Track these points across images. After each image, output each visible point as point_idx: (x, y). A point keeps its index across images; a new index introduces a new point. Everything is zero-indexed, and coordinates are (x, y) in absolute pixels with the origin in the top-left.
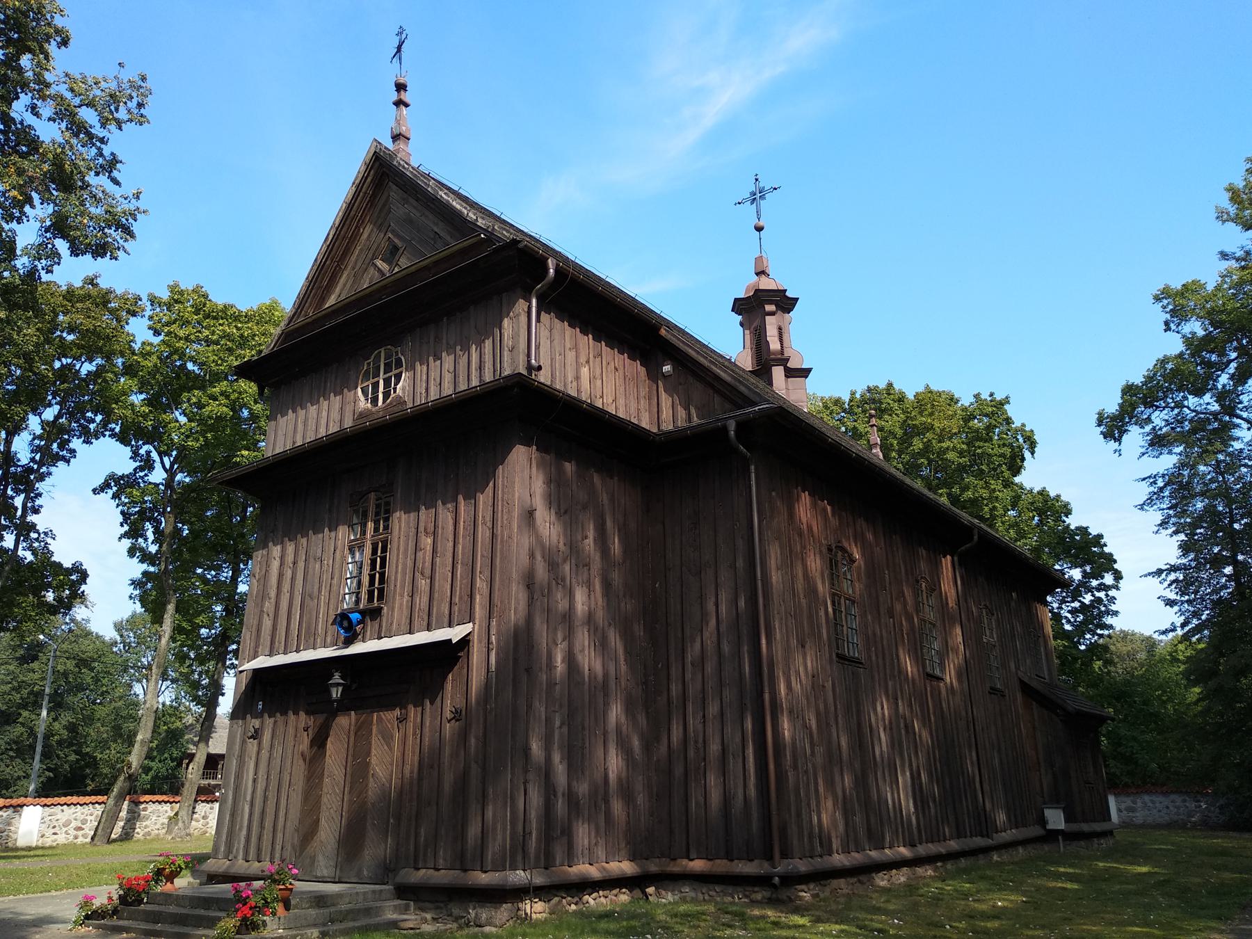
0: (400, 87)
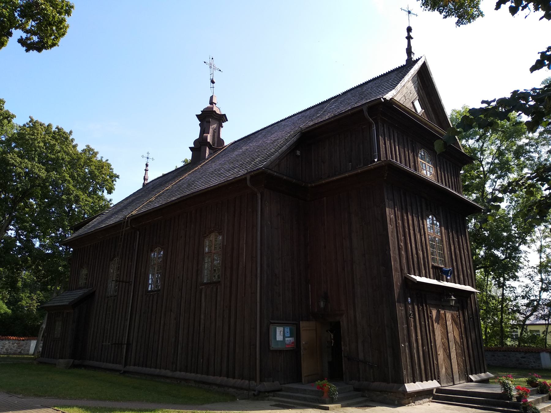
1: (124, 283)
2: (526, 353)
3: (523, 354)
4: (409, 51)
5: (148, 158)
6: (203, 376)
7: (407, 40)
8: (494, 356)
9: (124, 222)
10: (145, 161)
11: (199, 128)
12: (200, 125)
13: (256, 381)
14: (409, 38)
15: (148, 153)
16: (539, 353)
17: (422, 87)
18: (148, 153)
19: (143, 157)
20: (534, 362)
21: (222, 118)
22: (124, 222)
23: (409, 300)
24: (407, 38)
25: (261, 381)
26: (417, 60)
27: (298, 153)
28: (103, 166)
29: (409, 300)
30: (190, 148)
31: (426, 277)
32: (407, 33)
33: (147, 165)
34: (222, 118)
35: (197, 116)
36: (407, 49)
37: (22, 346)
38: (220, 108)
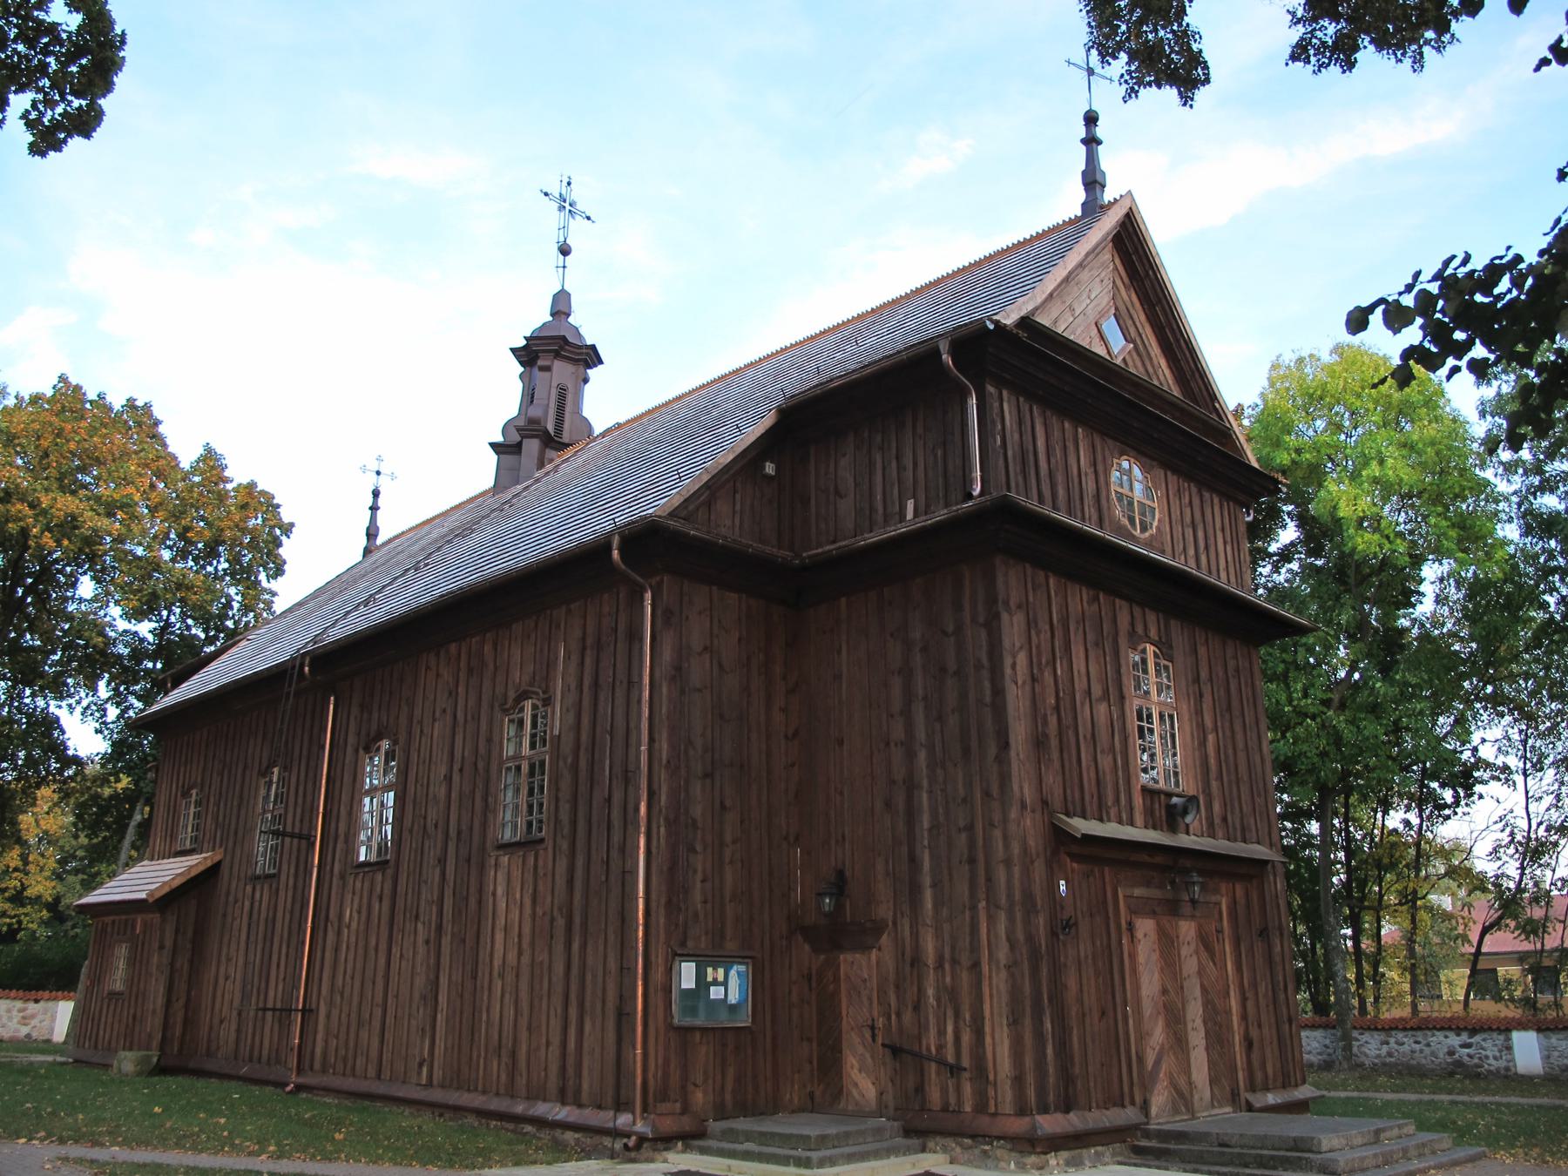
1: (296, 841)
2: (1473, 1032)
3: (1464, 1037)
4: (1093, 180)
5: (378, 473)
6: (587, 1112)
7: (1083, 149)
8: (1387, 1043)
9: (294, 667)
10: (370, 482)
11: (520, 385)
12: (521, 376)
13: (633, 1113)
14: (1091, 142)
15: (379, 459)
16: (1508, 1030)
17: (1126, 280)
18: (364, 469)
19: (364, 469)
20: (1495, 1058)
21: (590, 357)
22: (294, 667)
23: (1063, 888)
24: (1084, 141)
25: (645, 1109)
26: (1111, 205)
27: (770, 468)
28: (255, 500)
29: (1063, 888)
30: (494, 446)
31: (1120, 822)
32: (1084, 129)
33: (376, 494)
34: (590, 357)
35: (513, 350)
36: (1083, 173)
37: (33, 1016)
38: (588, 324)
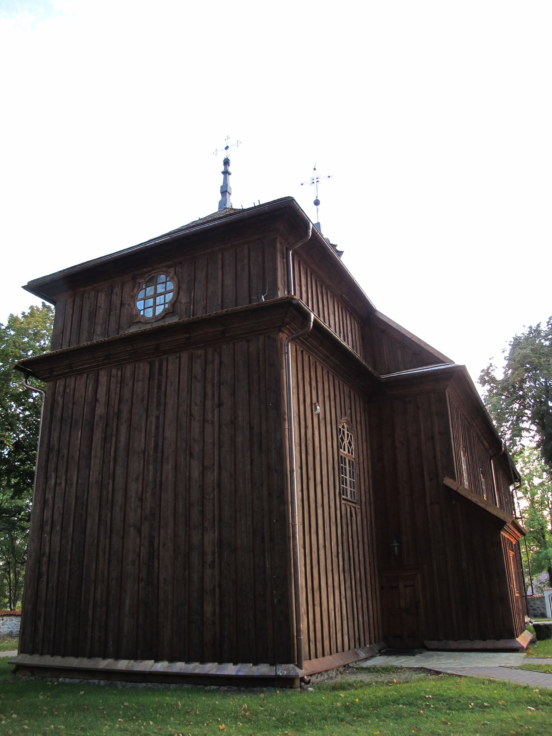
0: (226, 162)
4: (225, 191)
14: (226, 173)
